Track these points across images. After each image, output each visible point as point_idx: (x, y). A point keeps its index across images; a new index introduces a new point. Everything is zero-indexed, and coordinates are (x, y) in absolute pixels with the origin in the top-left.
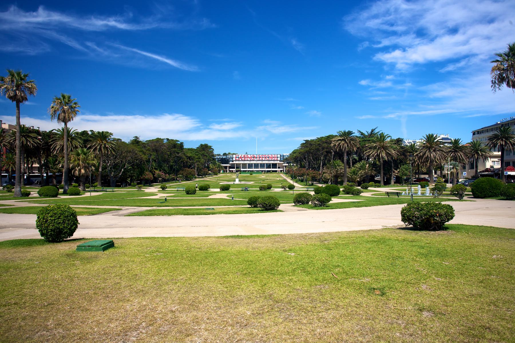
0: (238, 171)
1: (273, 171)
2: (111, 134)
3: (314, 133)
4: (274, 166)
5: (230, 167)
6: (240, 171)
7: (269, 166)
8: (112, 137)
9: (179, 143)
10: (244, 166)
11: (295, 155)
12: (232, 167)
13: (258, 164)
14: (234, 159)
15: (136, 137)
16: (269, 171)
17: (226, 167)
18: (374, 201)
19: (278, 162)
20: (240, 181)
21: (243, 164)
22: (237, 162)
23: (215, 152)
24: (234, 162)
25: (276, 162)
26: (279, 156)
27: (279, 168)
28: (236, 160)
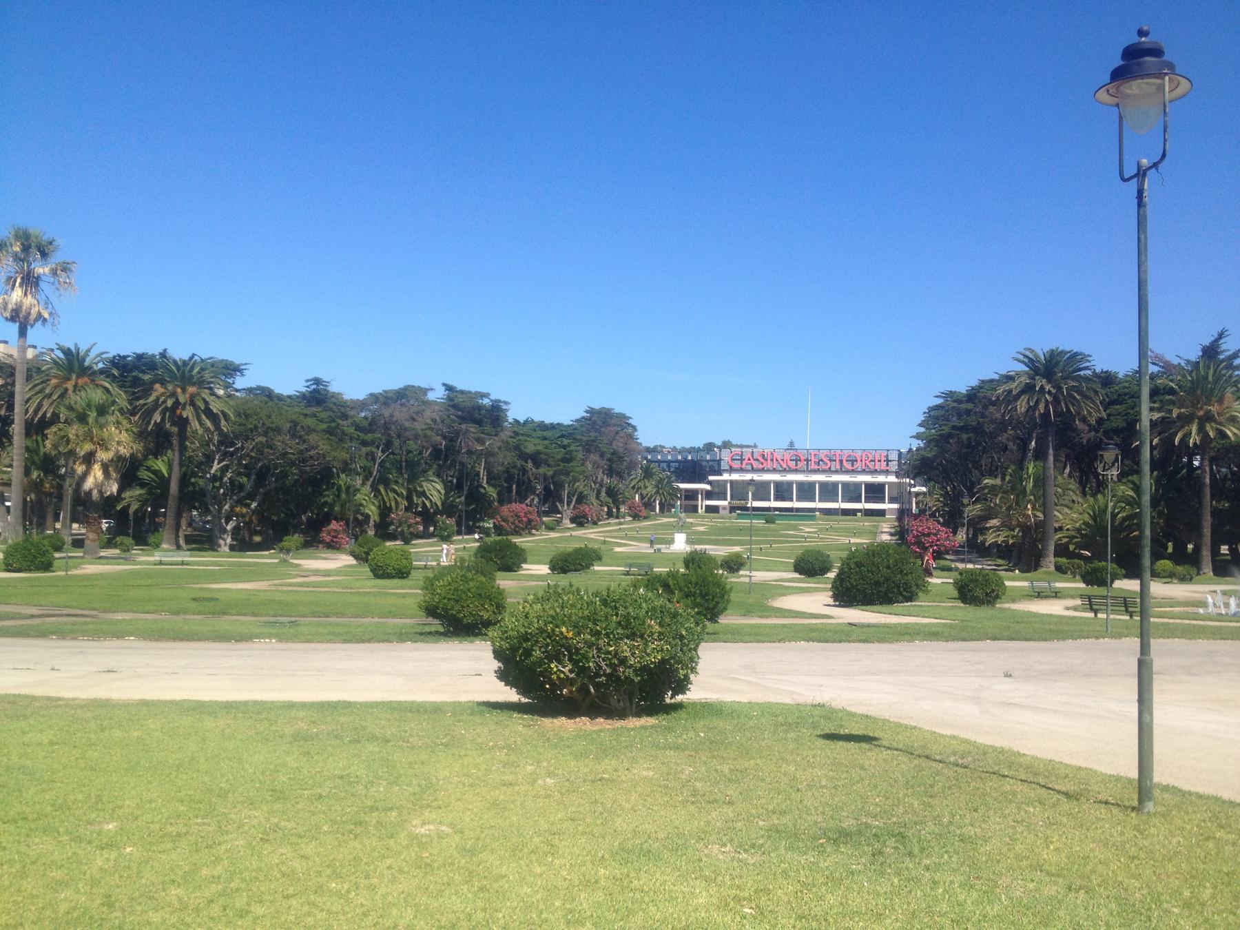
1: (846, 512)
2: (231, 369)
3: (982, 353)
5: (709, 495)
6: (747, 509)
8: (240, 382)
9: (486, 401)
10: (761, 490)
11: (399, 414)
13: (811, 485)
14: (724, 466)
15: (317, 381)
16: (853, 512)
17: (691, 495)
18: (177, 536)
20: (689, 542)
22: (735, 477)
23: (646, 438)
24: (726, 477)
25: (881, 479)
28: (731, 470)
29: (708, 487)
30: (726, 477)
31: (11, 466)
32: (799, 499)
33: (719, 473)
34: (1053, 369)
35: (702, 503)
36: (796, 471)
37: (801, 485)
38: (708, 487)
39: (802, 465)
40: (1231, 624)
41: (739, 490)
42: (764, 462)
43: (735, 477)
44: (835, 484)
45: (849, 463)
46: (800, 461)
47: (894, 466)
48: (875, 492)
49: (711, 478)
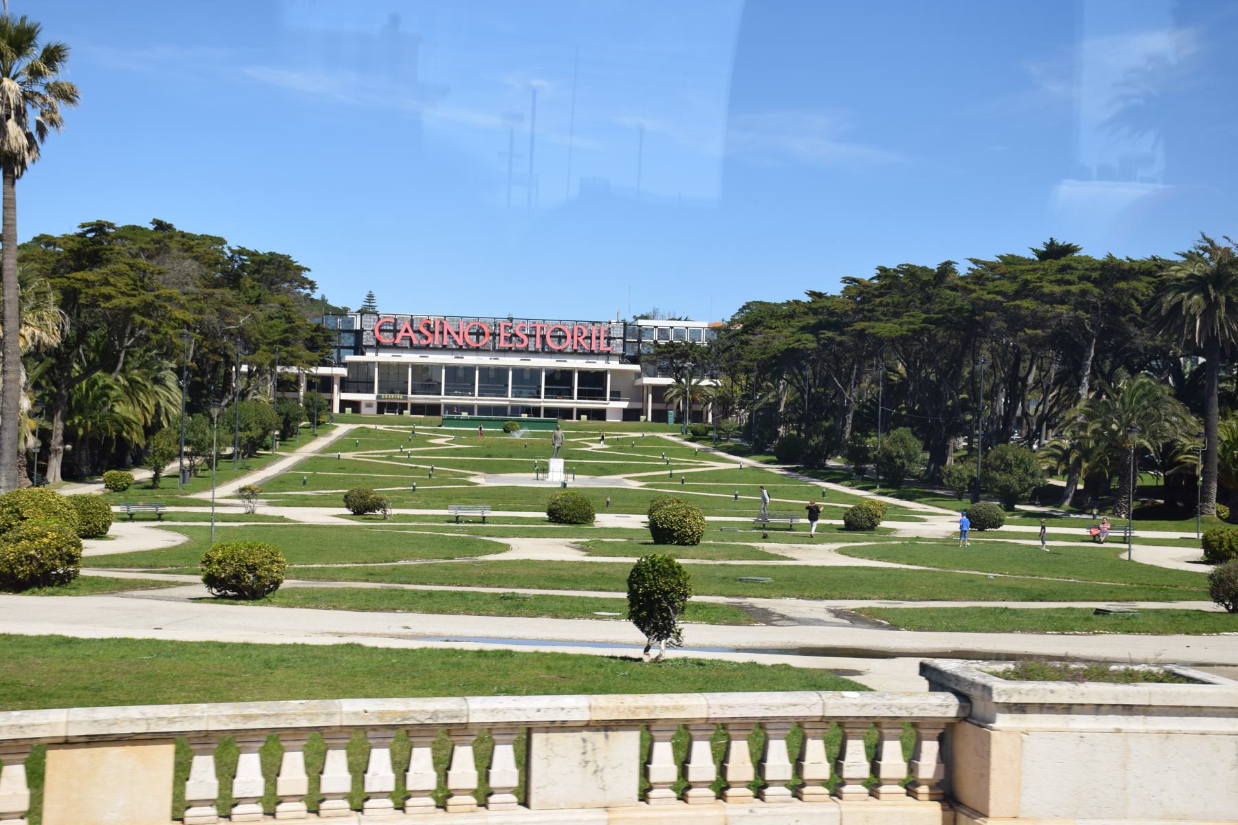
0: (392, 407)
4: (593, 383)
5: (345, 385)
7: (559, 382)
12: (358, 380)
13: (501, 372)
14: (368, 340)
19: (614, 364)
21: (417, 368)
22: (386, 357)
24: (370, 356)
25: (600, 364)
26: (618, 332)
27: (616, 396)
28: (379, 346)
29: (343, 371)
30: (370, 356)
32: (582, 395)
33: (358, 349)
36: (477, 350)
38: (343, 371)
42: (424, 334)
43: (386, 357)
45: (551, 339)
46: (483, 336)
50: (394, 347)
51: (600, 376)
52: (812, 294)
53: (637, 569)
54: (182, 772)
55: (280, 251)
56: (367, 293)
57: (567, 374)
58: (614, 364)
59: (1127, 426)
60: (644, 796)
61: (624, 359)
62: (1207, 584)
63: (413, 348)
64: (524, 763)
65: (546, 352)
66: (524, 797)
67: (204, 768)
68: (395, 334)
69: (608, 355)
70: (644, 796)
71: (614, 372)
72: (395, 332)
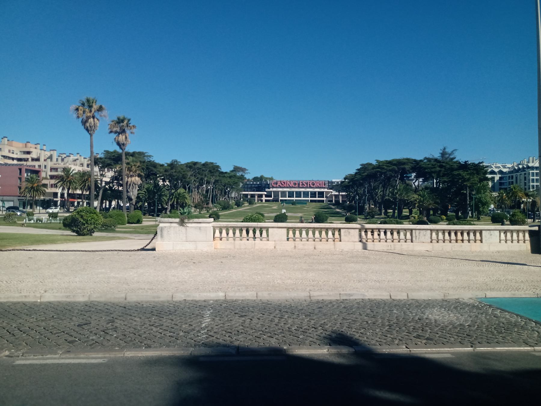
1: (319, 201)
13: (300, 192)
14: (271, 186)
16: (315, 201)
17: (261, 196)
19: (326, 190)
22: (275, 189)
24: (271, 190)
25: (322, 190)
28: (273, 187)
29: (266, 193)
30: (271, 190)
31: (512, 177)
32: (296, 197)
33: (269, 188)
34: (365, 167)
35: (264, 198)
36: (295, 188)
37: (304, 192)
38: (266, 193)
39: (297, 186)
40: (129, 354)
41: (276, 193)
42: (283, 184)
43: (275, 189)
44: (308, 192)
45: (312, 185)
46: (298, 184)
47: (327, 186)
48: (321, 194)
49: (266, 190)
50: (276, 187)
51: (323, 193)
52: (361, 165)
53: (276, 216)
54: (431, 234)
55: (209, 161)
56: (442, 148)
57: (315, 193)
58: (326, 190)
59: (119, 207)
60: (500, 242)
61: (327, 189)
62: (220, 217)
63: (280, 187)
64: (411, 235)
65: (310, 187)
66: (481, 241)
67: (434, 234)
68: (276, 184)
69: (324, 188)
70: (500, 242)
71: (326, 192)
72: (277, 184)
